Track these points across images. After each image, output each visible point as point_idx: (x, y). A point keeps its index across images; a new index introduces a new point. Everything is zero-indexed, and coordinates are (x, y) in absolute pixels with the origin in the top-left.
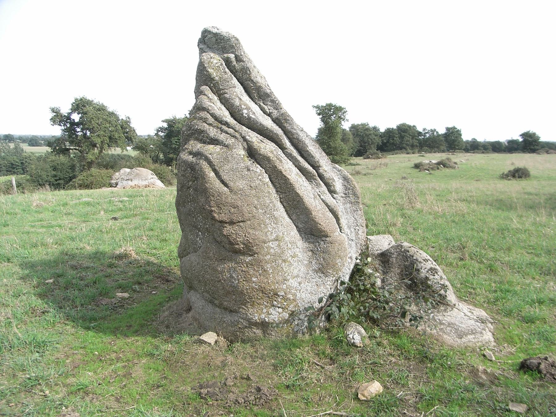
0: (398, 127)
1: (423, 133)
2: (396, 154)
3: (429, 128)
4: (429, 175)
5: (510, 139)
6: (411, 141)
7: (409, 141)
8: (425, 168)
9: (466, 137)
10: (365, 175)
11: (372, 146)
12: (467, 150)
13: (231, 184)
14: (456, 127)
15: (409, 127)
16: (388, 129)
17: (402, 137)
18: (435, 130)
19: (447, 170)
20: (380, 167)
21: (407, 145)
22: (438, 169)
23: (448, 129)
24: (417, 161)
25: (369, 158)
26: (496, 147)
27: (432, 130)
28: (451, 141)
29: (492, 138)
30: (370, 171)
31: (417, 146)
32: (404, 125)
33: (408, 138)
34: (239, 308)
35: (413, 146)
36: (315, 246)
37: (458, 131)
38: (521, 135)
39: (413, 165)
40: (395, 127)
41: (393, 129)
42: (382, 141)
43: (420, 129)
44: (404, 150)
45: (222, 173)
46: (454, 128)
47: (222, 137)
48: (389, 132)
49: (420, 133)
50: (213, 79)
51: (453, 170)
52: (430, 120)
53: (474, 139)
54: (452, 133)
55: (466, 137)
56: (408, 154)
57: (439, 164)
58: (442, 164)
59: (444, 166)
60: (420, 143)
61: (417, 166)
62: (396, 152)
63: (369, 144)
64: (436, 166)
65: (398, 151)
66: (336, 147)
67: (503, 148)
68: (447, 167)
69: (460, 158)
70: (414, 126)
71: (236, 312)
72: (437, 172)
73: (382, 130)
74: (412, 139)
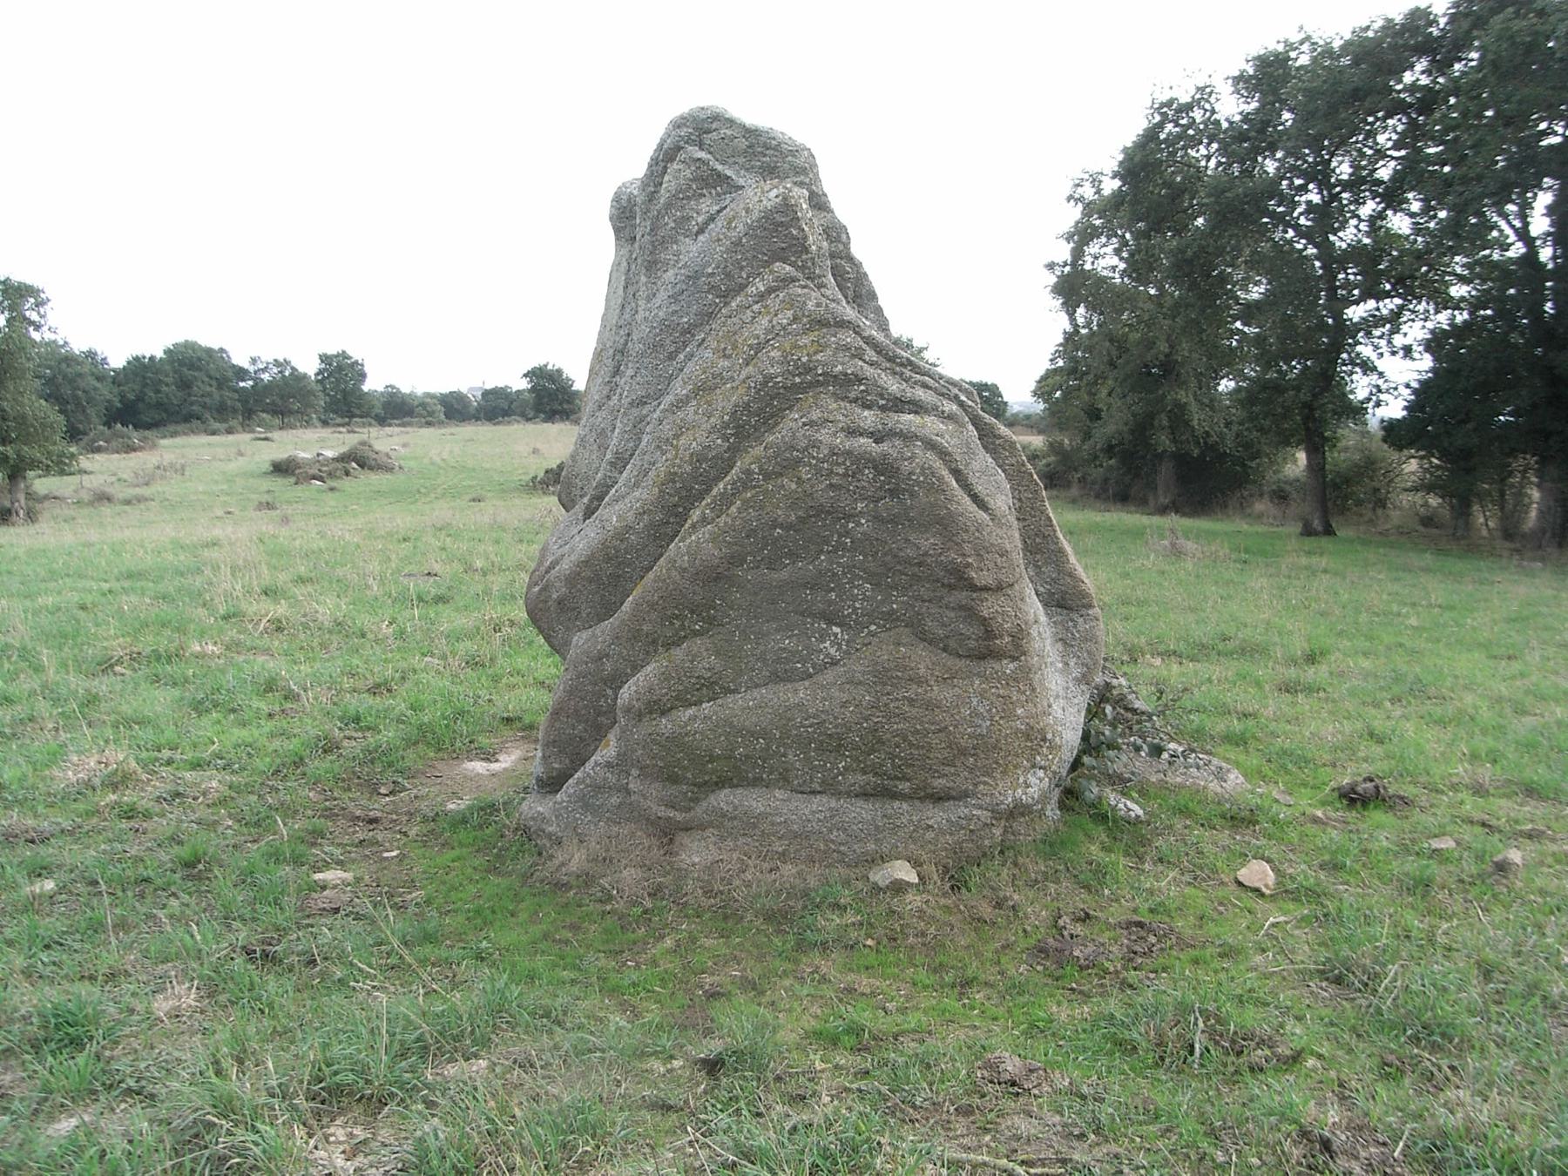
0: (168, 352)
1: (252, 369)
2: (174, 435)
3: (268, 356)
4: (330, 494)
5: (1033, 386)
6: (216, 396)
7: (210, 395)
8: (312, 472)
9: (374, 383)
10: (128, 502)
11: (91, 411)
12: (382, 421)
13: (992, 504)
14: (350, 352)
15: (209, 351)
16: (137, 359)
17: (185, 385)
18: (287, 362)
19: (375, 478)
20: (162, 478)
21: (204, 406)
22: (347, 474)
23: (324, 358)
24: (281, 455)
25: (99, 450)
26: (454, 409)
27: (277, 363)
28: (339, 393)
29: (442, 387)
30: (138, 491)
31: (235, 411)
32: (189, 346)
33: (202, 387)
34: (976, 785)
35: (222, 412)
36: (1067, 629)
37: (356, 362)
38: (525, 376)
39: (267, 467)
40: (159, 354)
41: (152, 358)
42: (123, 397)
43: (240, 359)
44: (196, 423)
45: (972, 479)
46: (344, 355)
47: (920, 393)
48: (139, 369)
49: (241, 373)
50: (806, 250)
51: (388, 476)
52: (265, 334)
53: (393, 387)
54: (340, 368)
55: (374, 383)
56: (214, 433)
57: (343, 458)
58: (359, 460)
59: (362, 466)
60: (245, 402)
61: (282, 469)
62: (171, 428)
63: (79, 404)
64: (339, 465)
65: (179, 428)
66: (24, 417)
67: (472, 411)
68: (371, 468)
69: (385, 440)
70: (222, 350)
71: (965, 795)
72: (346, 484)
73: (117, 361)
74: (220, 388)
